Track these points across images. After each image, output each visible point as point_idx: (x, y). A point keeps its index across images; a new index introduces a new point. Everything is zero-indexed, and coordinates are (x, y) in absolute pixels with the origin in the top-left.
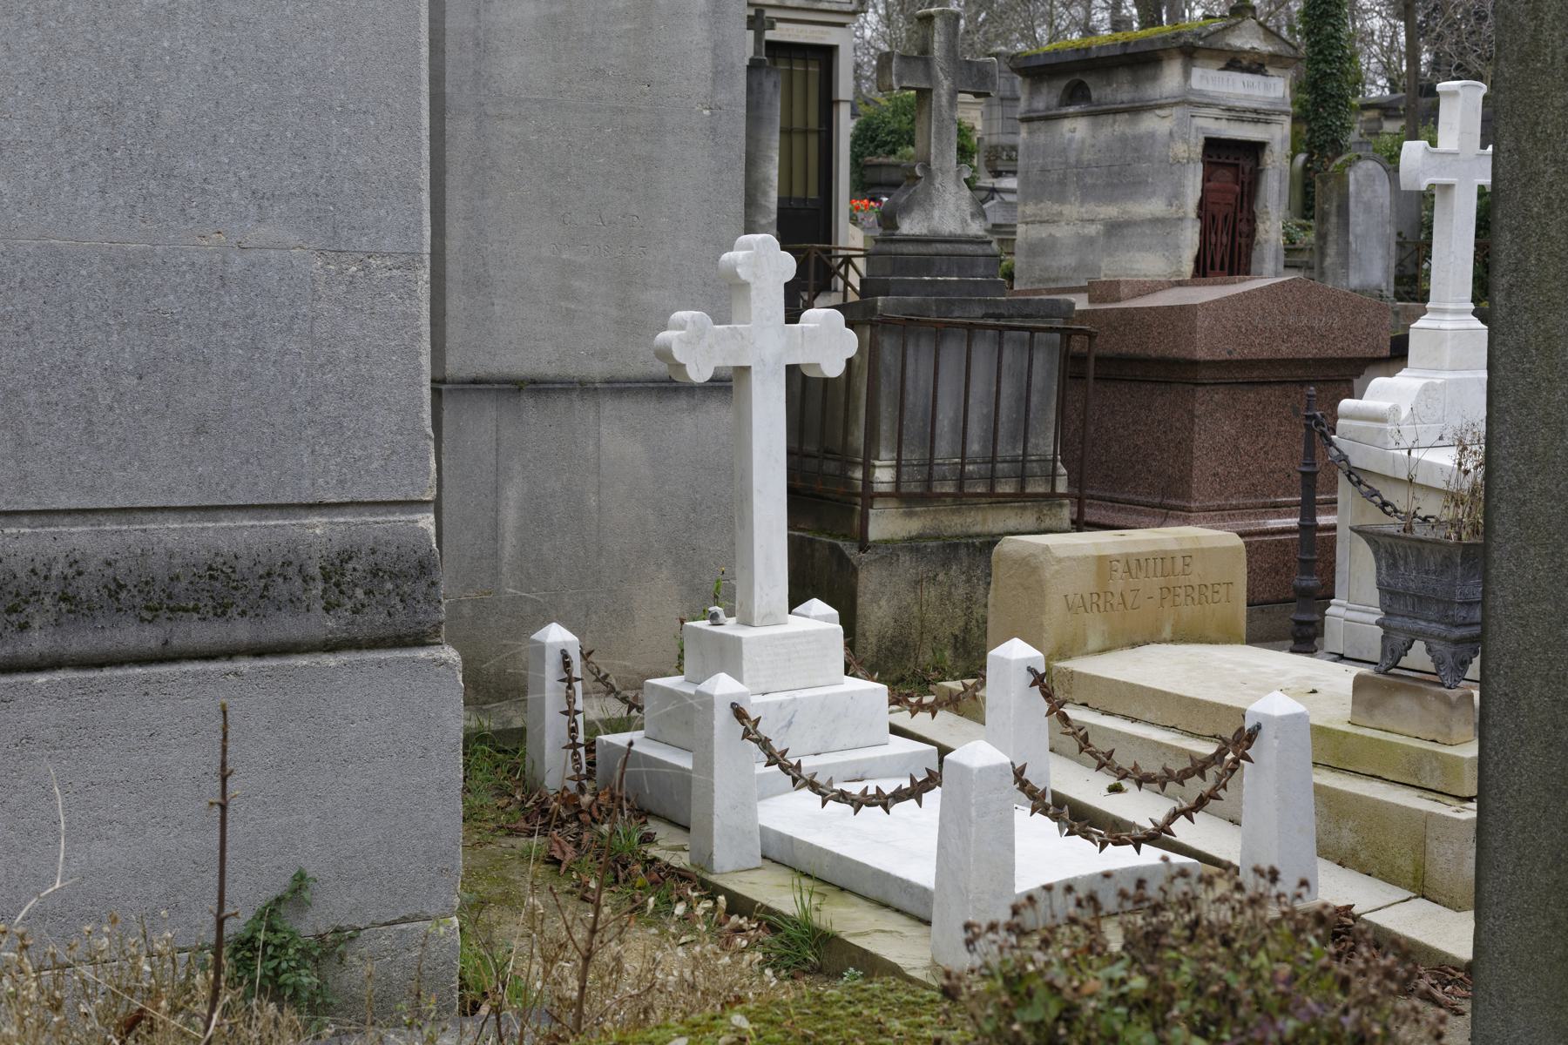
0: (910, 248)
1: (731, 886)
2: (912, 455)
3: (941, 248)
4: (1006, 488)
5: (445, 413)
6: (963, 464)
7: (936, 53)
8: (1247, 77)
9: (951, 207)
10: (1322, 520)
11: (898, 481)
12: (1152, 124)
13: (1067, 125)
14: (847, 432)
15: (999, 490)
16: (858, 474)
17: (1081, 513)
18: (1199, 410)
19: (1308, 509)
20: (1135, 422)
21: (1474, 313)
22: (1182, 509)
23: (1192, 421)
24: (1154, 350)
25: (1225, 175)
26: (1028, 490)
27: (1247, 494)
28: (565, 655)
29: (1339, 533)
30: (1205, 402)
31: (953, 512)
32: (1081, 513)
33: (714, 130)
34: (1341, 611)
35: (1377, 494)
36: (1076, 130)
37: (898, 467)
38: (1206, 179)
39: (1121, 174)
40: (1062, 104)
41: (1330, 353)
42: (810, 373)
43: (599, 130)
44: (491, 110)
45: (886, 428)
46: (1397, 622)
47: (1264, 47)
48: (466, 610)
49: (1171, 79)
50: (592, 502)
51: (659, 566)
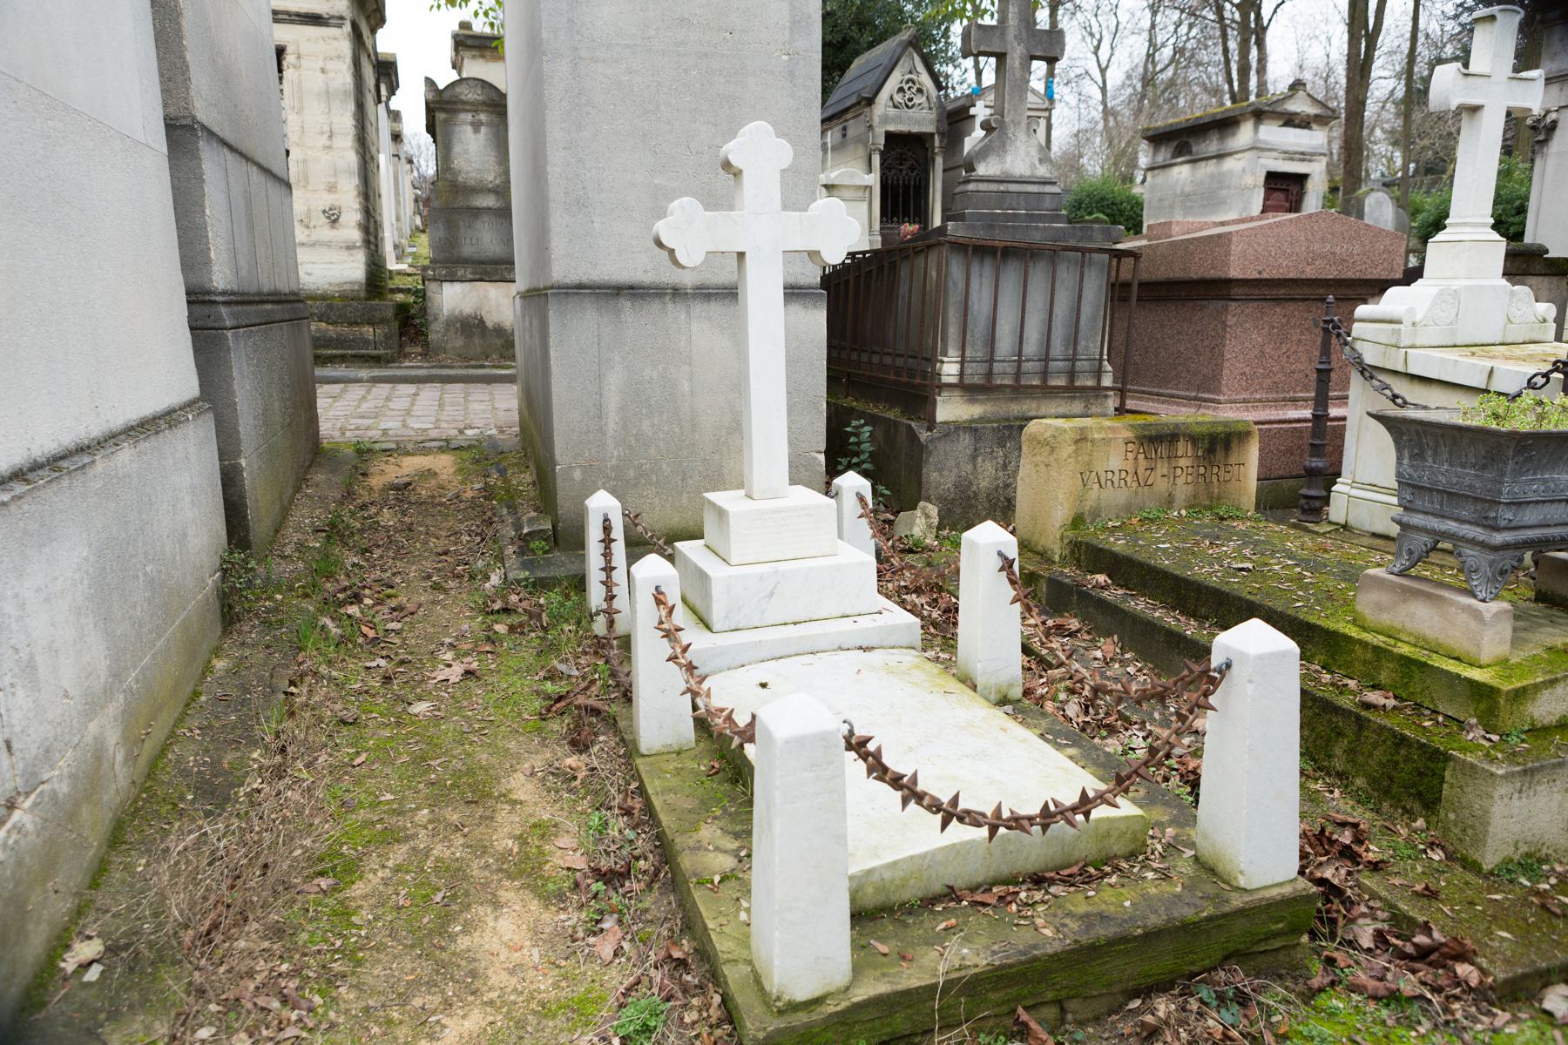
0: (983, 187)
1: (646, 781)
2: (976, 351)
3: (1013, 187)
6: (1019, 362)
7: (1011, 23)
9: (1022, 153)
10: (1334, 412)
11: (962, 374)
12: (1230, 164)
13: (1176, 170)
15: (1053, 382)
17: (1123, 403)
18: (1231, 321)
19: (1322, 401)
20: (1179, 333)
21: (1494, 227)
22: (1212, 401)
23: (1224, 330)
26: (1078, 384)
27: (1269, 390)
29: (1348, 423)
31: (1012, 400)
33: (792, 73)
34: (1346, 489)
35: (1388, 387)
36: (1182, 173)
37: (962, 363)
38: (1266, 199)
40: (1173, 157)
41: (1350, 275)
43: (686, 71)
44: (584, 54)
45: (953, 331)
46: (1417, 519)
47: (1312, 110)
48: (577, 474)
49: (1245, 134)
50: (686, 386)
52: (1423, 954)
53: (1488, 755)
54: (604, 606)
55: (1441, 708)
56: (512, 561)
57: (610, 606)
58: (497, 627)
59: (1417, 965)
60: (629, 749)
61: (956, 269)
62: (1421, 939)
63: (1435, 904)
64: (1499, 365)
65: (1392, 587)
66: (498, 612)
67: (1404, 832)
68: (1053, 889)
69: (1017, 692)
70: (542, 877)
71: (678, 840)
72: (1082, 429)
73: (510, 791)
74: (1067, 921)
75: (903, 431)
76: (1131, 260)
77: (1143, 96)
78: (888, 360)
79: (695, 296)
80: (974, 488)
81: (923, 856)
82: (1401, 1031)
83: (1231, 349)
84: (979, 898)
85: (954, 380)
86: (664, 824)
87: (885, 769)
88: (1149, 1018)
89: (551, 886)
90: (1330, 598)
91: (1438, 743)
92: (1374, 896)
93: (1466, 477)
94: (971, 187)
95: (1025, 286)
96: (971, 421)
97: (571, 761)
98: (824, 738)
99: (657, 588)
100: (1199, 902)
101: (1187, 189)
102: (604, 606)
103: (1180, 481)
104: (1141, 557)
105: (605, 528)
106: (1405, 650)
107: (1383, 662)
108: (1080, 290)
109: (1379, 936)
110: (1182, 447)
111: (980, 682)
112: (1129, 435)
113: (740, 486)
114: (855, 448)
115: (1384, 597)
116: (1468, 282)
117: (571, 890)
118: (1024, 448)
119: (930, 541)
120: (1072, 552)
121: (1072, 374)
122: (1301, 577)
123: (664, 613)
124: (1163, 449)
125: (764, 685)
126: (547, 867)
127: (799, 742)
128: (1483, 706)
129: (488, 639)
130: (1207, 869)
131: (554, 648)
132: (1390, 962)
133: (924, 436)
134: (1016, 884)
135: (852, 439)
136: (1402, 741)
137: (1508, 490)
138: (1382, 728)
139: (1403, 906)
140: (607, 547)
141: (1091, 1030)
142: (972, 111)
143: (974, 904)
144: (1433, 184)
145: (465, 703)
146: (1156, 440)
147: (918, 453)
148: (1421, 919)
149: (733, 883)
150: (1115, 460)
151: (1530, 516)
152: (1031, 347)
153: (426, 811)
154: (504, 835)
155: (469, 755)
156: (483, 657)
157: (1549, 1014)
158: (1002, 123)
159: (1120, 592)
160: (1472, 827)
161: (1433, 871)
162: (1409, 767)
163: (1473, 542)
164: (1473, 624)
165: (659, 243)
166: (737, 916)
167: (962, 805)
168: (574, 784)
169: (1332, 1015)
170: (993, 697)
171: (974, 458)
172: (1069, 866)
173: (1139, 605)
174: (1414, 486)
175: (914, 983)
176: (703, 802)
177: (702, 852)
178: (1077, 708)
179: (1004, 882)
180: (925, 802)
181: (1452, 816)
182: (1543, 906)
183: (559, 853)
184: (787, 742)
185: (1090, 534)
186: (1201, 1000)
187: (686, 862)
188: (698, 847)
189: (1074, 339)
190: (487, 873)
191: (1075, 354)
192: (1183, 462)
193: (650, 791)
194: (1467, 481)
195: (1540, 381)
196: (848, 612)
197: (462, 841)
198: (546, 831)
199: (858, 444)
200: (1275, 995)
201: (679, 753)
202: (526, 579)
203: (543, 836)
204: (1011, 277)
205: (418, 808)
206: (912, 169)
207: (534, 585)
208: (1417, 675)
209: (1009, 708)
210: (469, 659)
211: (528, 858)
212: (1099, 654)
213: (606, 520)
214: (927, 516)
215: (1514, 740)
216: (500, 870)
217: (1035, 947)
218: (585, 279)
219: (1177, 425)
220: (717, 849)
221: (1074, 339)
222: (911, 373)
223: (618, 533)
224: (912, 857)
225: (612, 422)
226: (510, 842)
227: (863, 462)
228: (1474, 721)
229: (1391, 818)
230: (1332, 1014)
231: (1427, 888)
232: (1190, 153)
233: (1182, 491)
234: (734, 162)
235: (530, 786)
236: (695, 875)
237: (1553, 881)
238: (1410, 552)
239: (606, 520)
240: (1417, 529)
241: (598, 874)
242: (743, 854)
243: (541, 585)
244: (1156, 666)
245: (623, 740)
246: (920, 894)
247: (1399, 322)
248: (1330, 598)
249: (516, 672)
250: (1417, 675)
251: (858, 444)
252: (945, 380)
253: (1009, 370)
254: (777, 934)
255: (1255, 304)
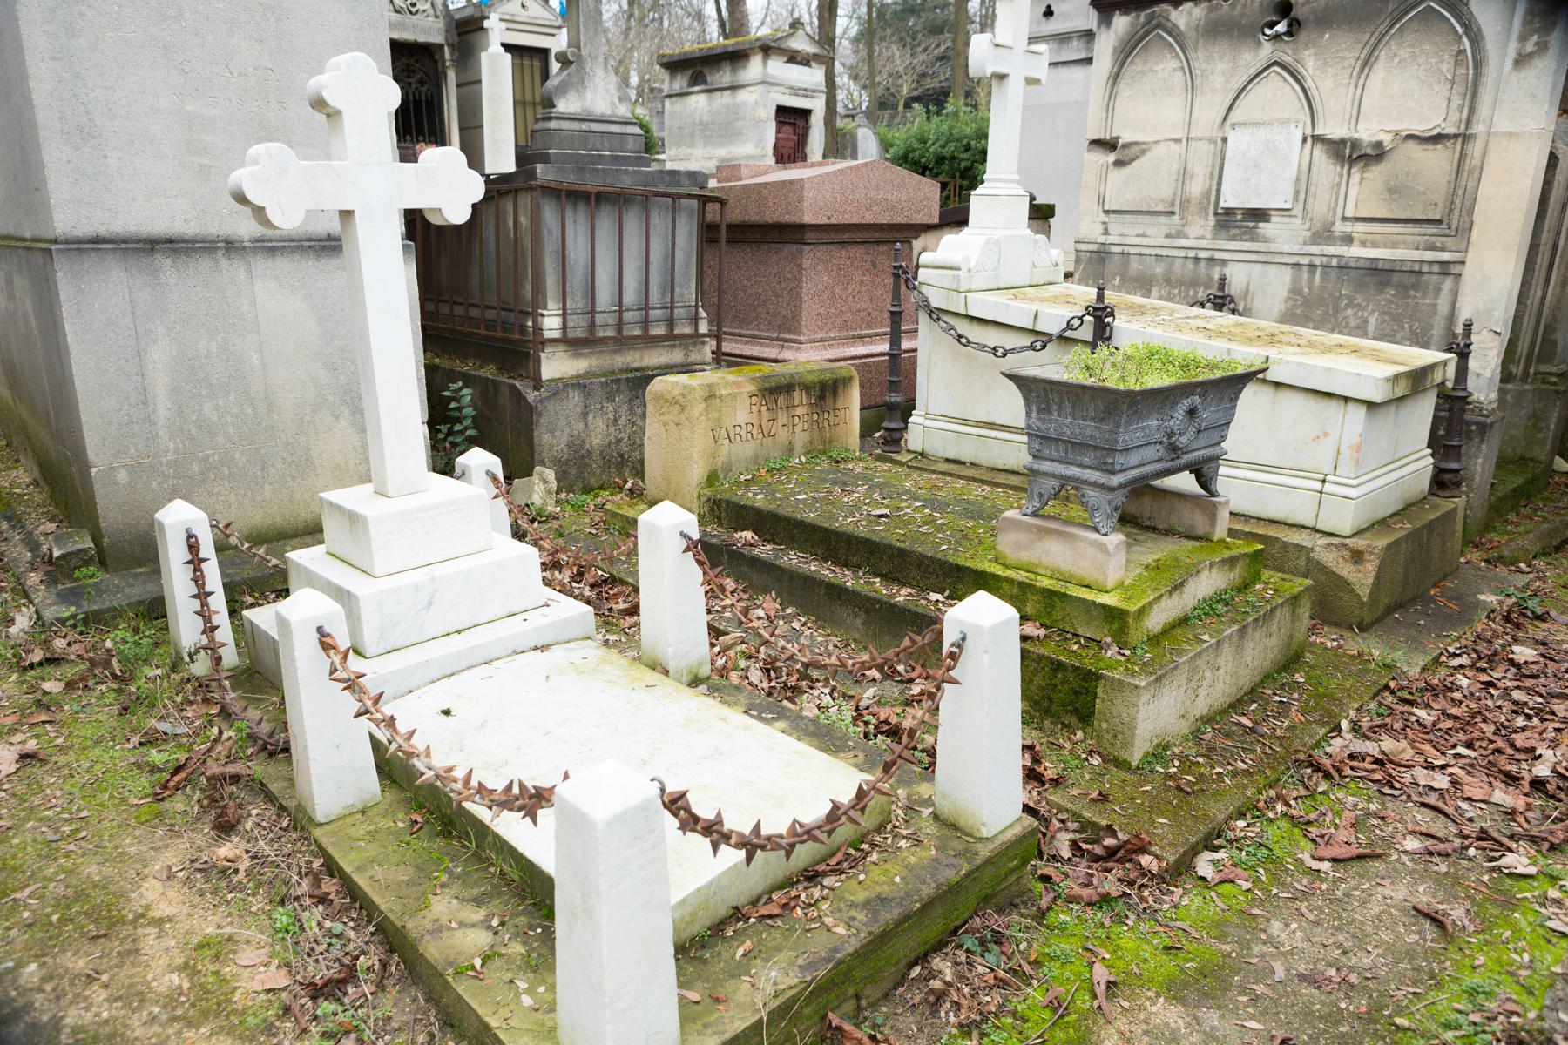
0: (565, 125)
2: (576, 303)
4: (659, 330)
5: (59, 275)
6: (621, 312)
8: (800, 68)
10: (905, 345)
11: (564, 328)
12: (743, 96)
13: (693, 98)
14: (518, 284)
16: (530, 323)
17: (719, 346)
18: (806, 264)
19: (895, 340)
22: (795, 341)
24: (771, 216)
25: (788, 129)
26: (676, 332)
27: (841, 328)
28: (191, 537)
30: (810, 257)
31: (615, 352)
32: (719, 346)
34: (921, 420)
36: (698, 102)
37: (564, 316)
38: (778, 132)
39: (725, 129)
41: (899, 220)
42: (434, 220)
45: (551, 282)
46: (1046, 466)
48: (122, 476)
49: (755, 67)
50: (255, 359)
51: (337, 417)
52: (1111, 853)
53: (1127, 669)
54: (205, 640)
55: (1080, 632)
56: (41, 594)
57: (212, 640)
58: (47, 686)
59: (1110, 865)
60: (298, 821)
61: (549, 215)
62: (1109, 842)
63: (1107, 805)
64: (1045, 309)
65: (1029, 527)
66: (40, 664)
67: (1068, 745)
68: (826, 882)
69: (705, 670)
70: (235, 1012)
71: (410, 925)
72: (710, 386)
73: (147, 908)
74: (853, 913)
75: (507, 391)
76: (717, 206)
77: (631, 15)
78: (474, 312)
79: (255, 250)
80: (587, 446)
81: (709, 885)
82: (1116, 929)
83: (808, 288)
84: (764, 911)
85: (557, 335)
86: (383, 907)
87: (696, 819)
88: (936, 984)
89: (252, 1021)
90: (966, 537)
91: (1089, 664)
92: (1061, 809)
93: (1087, 429)
94: (553, 125)
95: (621, 233)
96: (578, 377)
97: (225, 851)
98: (643, 807)
99: (320, 629)
100: (955, 861)
101: (706, 118)
102: (205, 640)
103: (798, 429)
104: (786, 511)
105: (190, 547)
106: (1045, 583)
107: (1029, 595)
108: (673, 237)
109: (1075, 845)
110: (799, 396)
111: (671, 667)
112: (752, 388)
113: (366, 479)
114: (456, 414)
115: (1023, 537)
116: (1010, 232)
117: (279, 1017)
118: (650, 407)
119: (551, 508)
120: (712, 510)
121: (671, 322)
122: (934, 520)
123: (337, 660)
124: (782, 400)
125: (447, 713)
126: (237, 996)
127: (621, 820)
128: (1115, 627)
129: (39, 704)
130: (949, 825)
131: (147, 702)
132: (1090, 867)
133: (531, 396)
134: (792, 885)
135: (453, 405)
136: (1059, 666)
137: (1123, 439)
138: (1041, 657)
139: (1087, 815)
140: (197, 569)
141: (884, 1009)
142: (486, 24)
143: (762, 918)
144: (892, 117)
145: (37, 801)
146: (776, 391)
147: (525, 416)
148: (1104, 823)
149: (498, 962)
150: (742, 412)
151: (1134, 458)
152: (630, 297)
153: (33, 967)
154: (161, 967)
155: (69, 872)
156: (38, 730)
157: (1203, 879)
158: (579, 56)
159: (769, 547)
160: (1122, 732)
161: (1098, 776)
162: (1067, 688)
163: (1095, 485)
164: (1100, 556)
165: (241, 198)
166: (519, 1003)
167: (765, 832)
168: (236, 879)
169: (1064, 929)
170: (684, 679)
171: (585, 415)
172: (834, 854)
173: (792, 560)
174: (1042, 437)
175: (739, 1026)
176: (419, 869)
177: (445, 934)
178: (759, 673)
179: (780, 887)
180: (733, 842)
181: (1104, 725)
182: (1178, 788)
183: (246, 973)
184: (609, 823)
185: (725, 489)
186: (968, 951)
187: (432, 950)
188: (438, 930)
189: (670, 285)
190: (156, 1029)
191: (672, 301)
192: (800, 411)
193: (348, 869)
194: (1088, 432)
195: (1076, 323)
196: (514, 610)
197: (104, 994)
198: (220, 948)
199: (459, 409)
200: (1015, 924)
201: (363, 812)
202: (73, 616)
203: (217, 957)
204: (605, 223)
205: (20, 965)
206: (422, 82)
207: (85, 622)
208: (1058, 605)
209: (703, 688)
210: (19, 737)
211: (207, 992)
212: (760, 613)
213: (190, 536)
214: (545, 482)
215: (1139, 652)
216: (174, 1019)
217: (835, 950)
218: (102, 231)
219: (792, 375)
220: (462, 924)
221: (670, 285)
222: (506, 327)
223: (207, 550)
224: (699, 890)
225: (163, 408)
226: (175, 977)
227: (466, 428)
228: (1109, 640)
229: (1052, 733)
230: (1063, 928)
231: (1100, 794)
232: (705, 82)
233: (801, 439)
234: (328, 96)
235: (171, 893)
236: (450, 964)
237: (1177, 763)
238: (1041, 495)
239: (190, 536)
240: (1046, 474)
241: (318, 992)
242: (495, 923)
243: (96, 621)
244: (818, 618)
245: (283, 808)
246: (708, 923)
247: (958, 269)
248: (966, 537)
249: (97, 742)
250: (1058, 605)
251: (459, 409)
252: (548, 334)
253: (610, 321)
254: (609, 1027)
255: (824, 248)
